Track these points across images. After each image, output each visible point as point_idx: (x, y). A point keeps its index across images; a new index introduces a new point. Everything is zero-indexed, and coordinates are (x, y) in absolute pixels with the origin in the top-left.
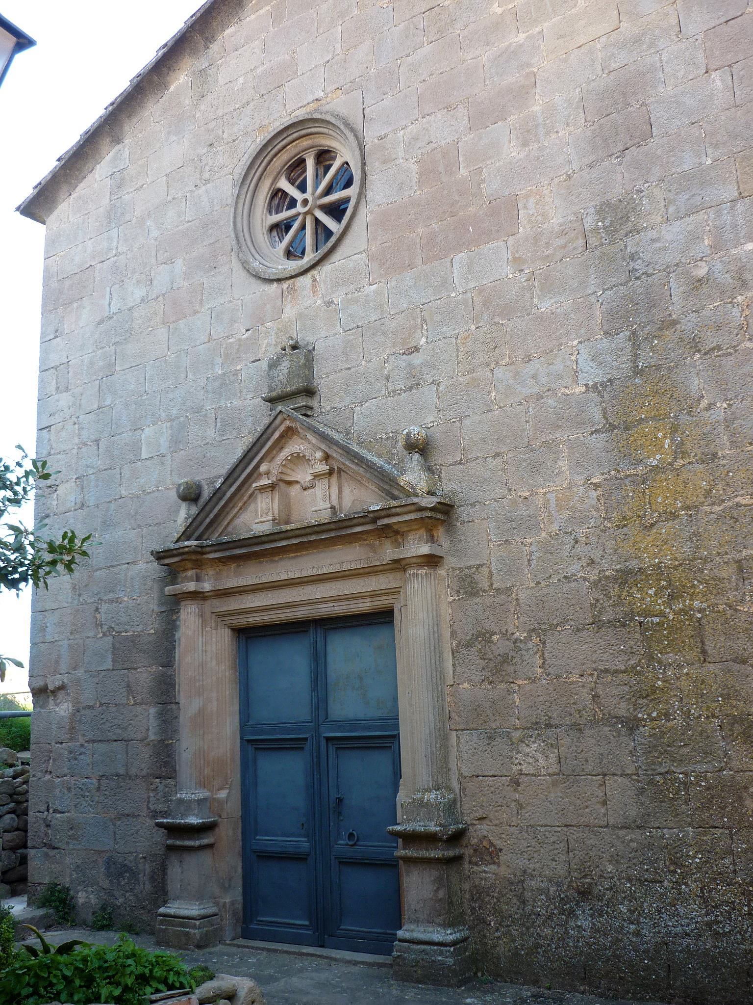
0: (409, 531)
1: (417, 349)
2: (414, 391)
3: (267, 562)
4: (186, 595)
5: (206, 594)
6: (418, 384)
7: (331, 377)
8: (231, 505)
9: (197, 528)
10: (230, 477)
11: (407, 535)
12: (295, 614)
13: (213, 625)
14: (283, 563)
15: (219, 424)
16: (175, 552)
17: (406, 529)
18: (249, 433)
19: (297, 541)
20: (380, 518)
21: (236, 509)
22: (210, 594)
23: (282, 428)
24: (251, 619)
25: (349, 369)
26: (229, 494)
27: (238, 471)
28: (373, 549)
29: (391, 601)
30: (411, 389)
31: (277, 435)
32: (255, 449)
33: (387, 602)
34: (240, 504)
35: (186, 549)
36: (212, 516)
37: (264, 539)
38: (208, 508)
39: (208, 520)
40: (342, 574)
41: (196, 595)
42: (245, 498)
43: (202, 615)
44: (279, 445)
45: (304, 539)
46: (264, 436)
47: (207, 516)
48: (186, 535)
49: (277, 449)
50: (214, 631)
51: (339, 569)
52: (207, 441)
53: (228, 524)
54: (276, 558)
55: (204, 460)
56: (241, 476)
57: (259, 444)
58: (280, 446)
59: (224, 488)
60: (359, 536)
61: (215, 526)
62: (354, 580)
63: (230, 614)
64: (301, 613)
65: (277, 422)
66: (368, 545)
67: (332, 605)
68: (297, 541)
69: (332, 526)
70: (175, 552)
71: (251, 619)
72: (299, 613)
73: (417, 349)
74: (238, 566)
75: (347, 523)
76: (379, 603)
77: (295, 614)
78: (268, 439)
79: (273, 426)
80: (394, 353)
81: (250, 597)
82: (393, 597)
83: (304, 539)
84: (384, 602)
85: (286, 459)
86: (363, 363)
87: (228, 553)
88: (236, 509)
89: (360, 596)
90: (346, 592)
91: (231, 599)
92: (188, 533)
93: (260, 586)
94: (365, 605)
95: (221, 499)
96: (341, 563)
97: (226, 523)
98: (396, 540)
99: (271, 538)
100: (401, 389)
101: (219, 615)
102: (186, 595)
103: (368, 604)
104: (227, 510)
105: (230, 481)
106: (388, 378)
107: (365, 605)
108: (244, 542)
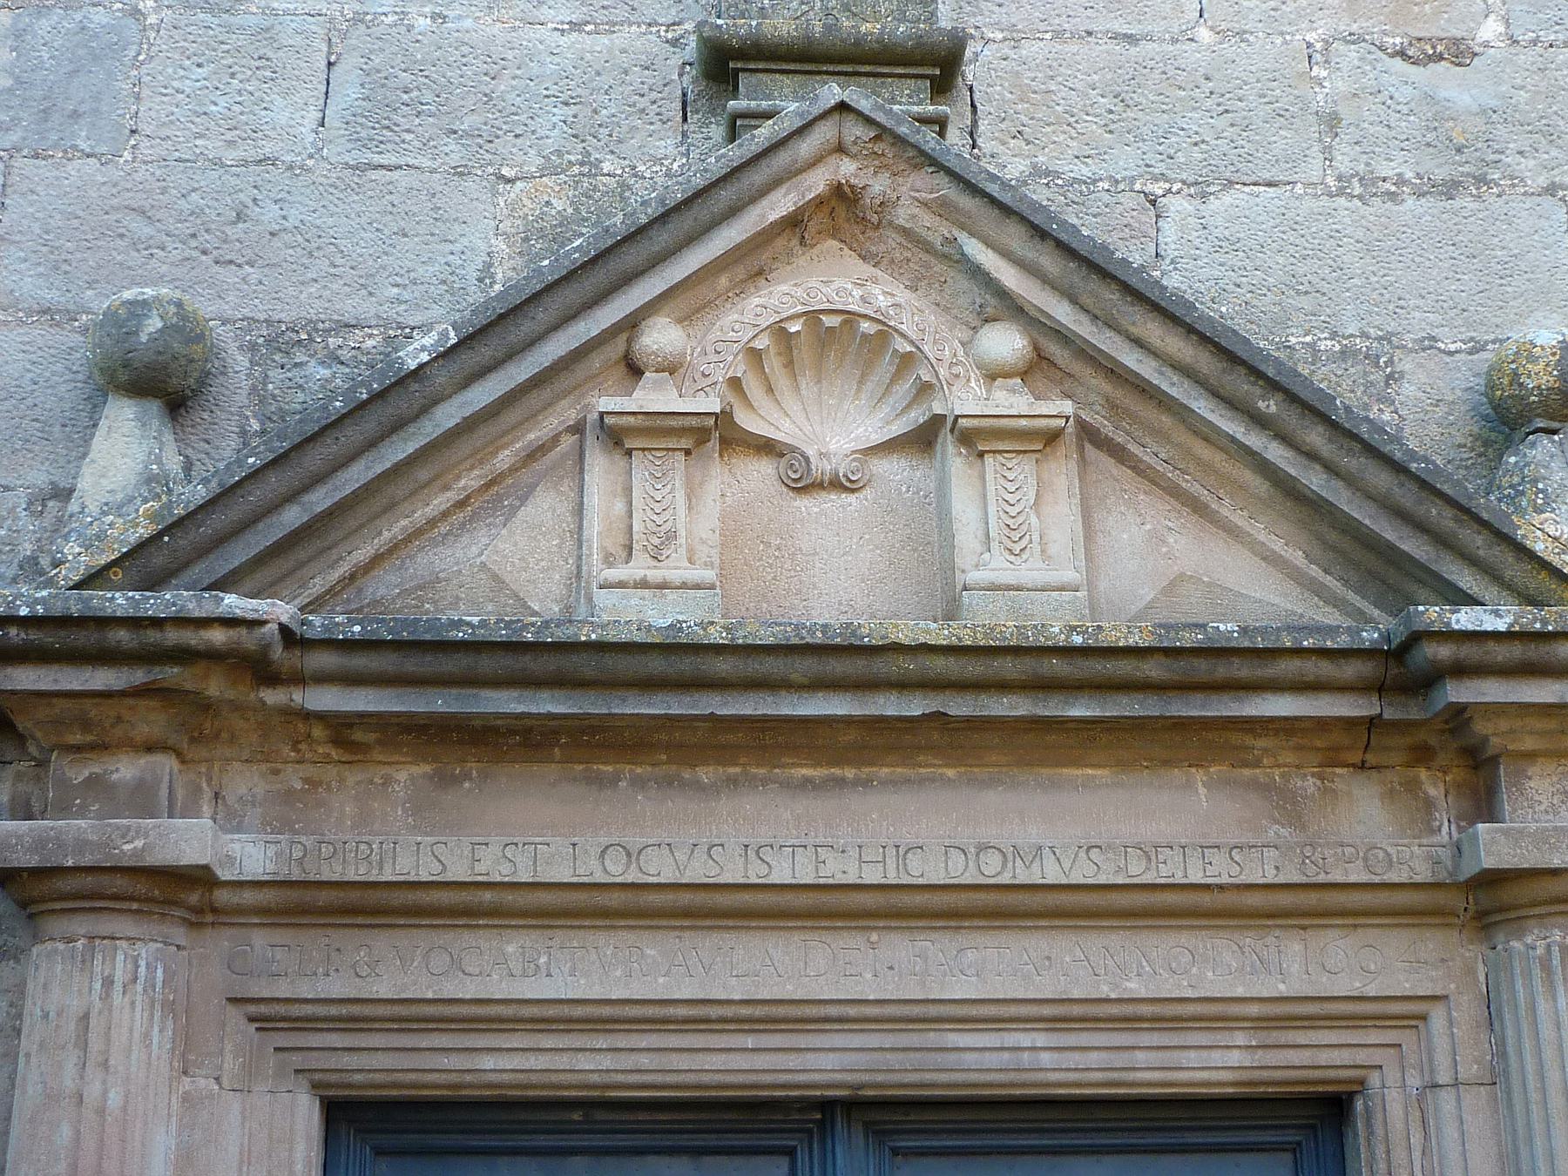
0: (1531, 756)
1: (1459, 53)
2: (1464, 202)
3: (639, 783)
4: (120, 883)
5: (222, 897)
6: (1481, 180)
7: (1029, 49)
8: (423, 474)
9: (221, 540)
10: (491, 334)
11: (1519, 776)
12: (793, 1061)
13: (230, 1064)
14: (749, 803)
15: (348, 91)
16: (122, 636)
17: (1529, 744)
18: (548, 170)
19: (916, 706)
20: (1461, 670)
21: (441, 502)
22: (249, 897)
23: (817, 183)
24: (488, 1062)
25: (1131, 39)
26: (448, 415)
27: (541, 316)
28: (1290, 809)
29: (1361, 1057)
30: (1450, 189)
31: (780, 205)
32: (662, 238)
33: (1344, 1057)
34: (470, 481)
35: (218, 636)
36: (320, 499)
37: (723, 666)
38: (315, 458)
39: (293, 517)
40: (1141, 899)
41: (182, 894)
42: (504, 458)
43: (179, 1010)
44: (751, 263)
45: (960, 706)
46: (726, 195)
47: (292, 497)
48: (145, 563)
49: (740, 272)
50: (234, 1104)
51: (1137, 871)
52: (268, 149)
53: (376, 560)
54: (705, 774)
55: (233, 232)
56: (550, 338)
57: (686, 222)
58: (753, 263)
59: (441, 378)
60: (1236, 738)
61: (301, 554)
62: (1184, 938)
63: (356, 1017)
64: (825, 1063)
65: (806, 147)
66: (1265, 788)
67: (1025, 1040)
68: (916, 706)
69: (1152, 670)
70: (122, 636)
71: (488, 1062)
72: (811, 1060)
73: (1459, 53)
74: (444, 780)
75: (1242, 670)
76: (1294, 1057)
77: (793, 1061)
78: (733, 212)
79: (782, 159)
80: (1354, 39)
81: (514, 945)
82: (1374, 1037)
83: (960, 706)
84: (1324, 1057)
85: (812, 317)
86: (1204, 34)
87: (439, 703)
88: (441, 502)
89: (1214, 1016)
90: (1135, 987)
91: (381, 942)
92: (158, 559)
93: (615, 899)
94: (1217, 1058)
95: (398, 426)
96: (1149, 852)
97: (362, 554)
98: (1412, 786)
99: (1202, 667)
100: (1401, 181)
101: (269, 1018)
102: (120, 883)
103: (1235, 1058)
104: (399, 489)
105: (484, 352)
106: (1332, 122)
107: (1217, 1058)
108: (586, 666)
